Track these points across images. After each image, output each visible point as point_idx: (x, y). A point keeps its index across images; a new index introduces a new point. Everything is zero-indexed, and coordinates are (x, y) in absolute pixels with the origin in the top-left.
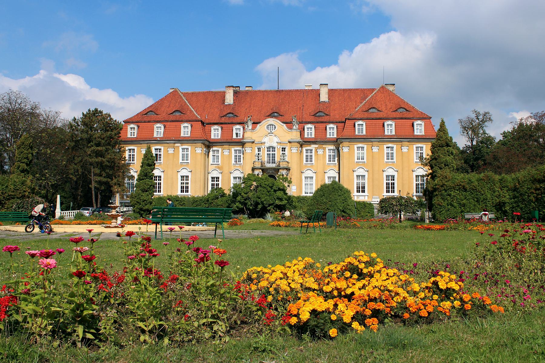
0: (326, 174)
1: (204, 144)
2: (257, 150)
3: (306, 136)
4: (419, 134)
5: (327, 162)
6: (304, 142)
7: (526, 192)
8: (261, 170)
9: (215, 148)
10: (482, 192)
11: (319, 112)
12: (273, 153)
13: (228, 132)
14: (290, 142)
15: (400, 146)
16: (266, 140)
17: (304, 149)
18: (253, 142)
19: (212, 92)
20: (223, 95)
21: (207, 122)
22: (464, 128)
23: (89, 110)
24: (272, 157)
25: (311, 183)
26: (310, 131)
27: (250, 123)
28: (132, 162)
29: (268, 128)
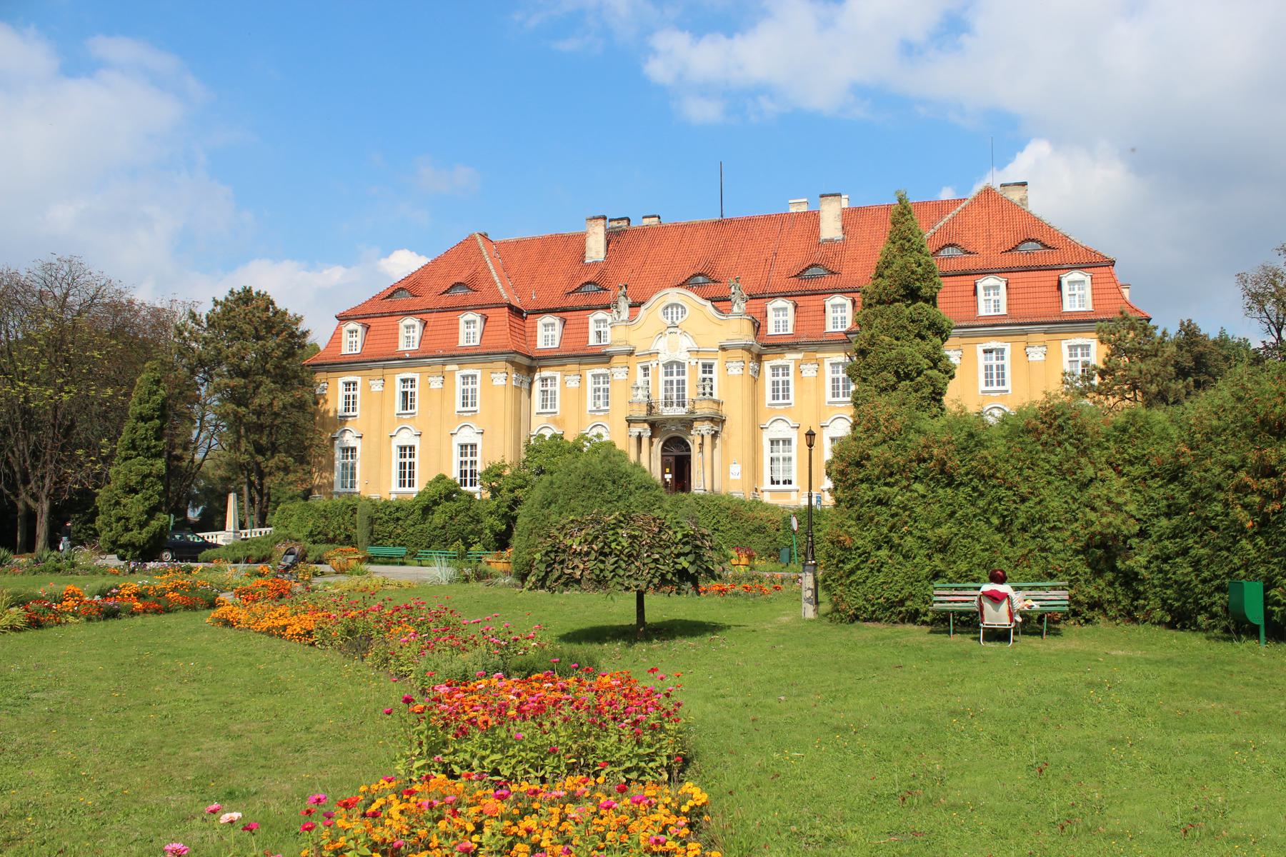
0: (394, 439)
1: (512, 363)
2: (640, 372)
3: (771, 330)
4: (1077, 309)
5: (829, 397)
6: (763, 348)
7: (1219, 487)
8: (646, 426)
9: (546, 373)
10: (1024, 489)
11: (812, 266)
12: (681, 378)
13: (573, 331)
14: (723, 349)
15: (1023, 345)
16: (661, 345)
17: (767, 366)
18: (631, 353)
19: (563, 236)
20: (580, 241)
21: (532, 307)
22: (1255, 296)
23: (232, 292)
24: (678, 390)
25: (787, 455)
26: (780, 317)
27: (624, 305)
28: (351, 413)
29: (665, 314)
